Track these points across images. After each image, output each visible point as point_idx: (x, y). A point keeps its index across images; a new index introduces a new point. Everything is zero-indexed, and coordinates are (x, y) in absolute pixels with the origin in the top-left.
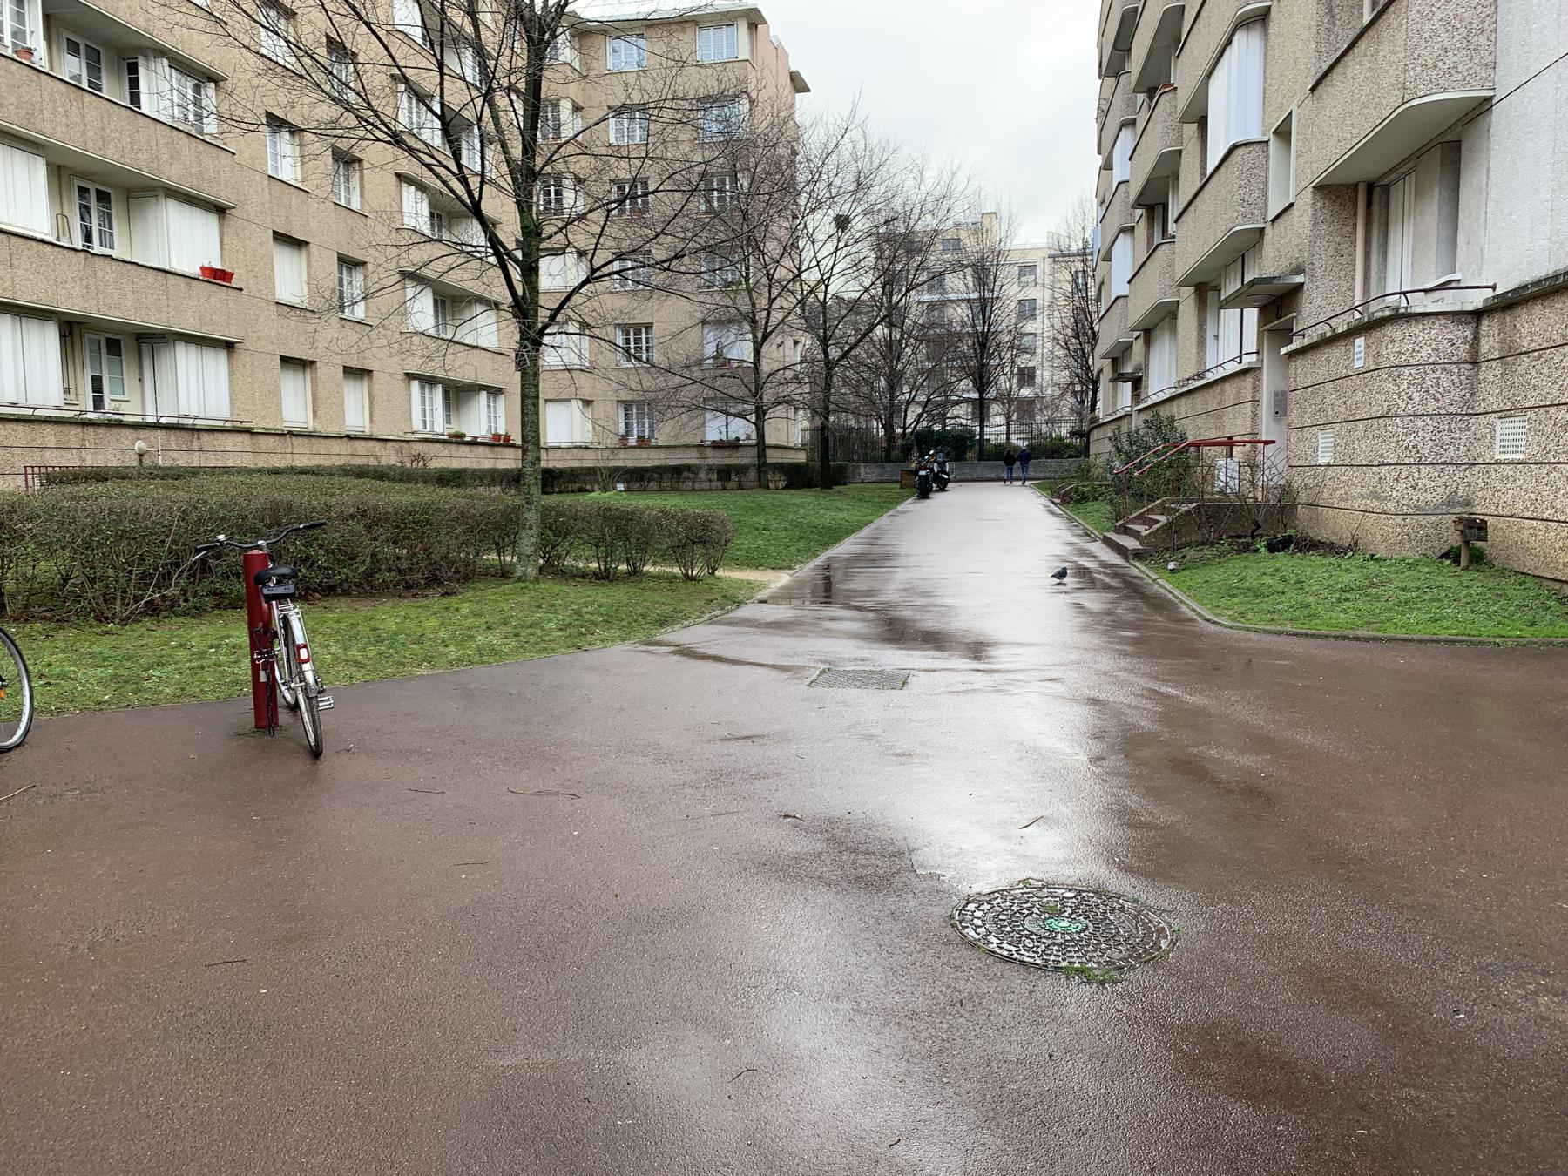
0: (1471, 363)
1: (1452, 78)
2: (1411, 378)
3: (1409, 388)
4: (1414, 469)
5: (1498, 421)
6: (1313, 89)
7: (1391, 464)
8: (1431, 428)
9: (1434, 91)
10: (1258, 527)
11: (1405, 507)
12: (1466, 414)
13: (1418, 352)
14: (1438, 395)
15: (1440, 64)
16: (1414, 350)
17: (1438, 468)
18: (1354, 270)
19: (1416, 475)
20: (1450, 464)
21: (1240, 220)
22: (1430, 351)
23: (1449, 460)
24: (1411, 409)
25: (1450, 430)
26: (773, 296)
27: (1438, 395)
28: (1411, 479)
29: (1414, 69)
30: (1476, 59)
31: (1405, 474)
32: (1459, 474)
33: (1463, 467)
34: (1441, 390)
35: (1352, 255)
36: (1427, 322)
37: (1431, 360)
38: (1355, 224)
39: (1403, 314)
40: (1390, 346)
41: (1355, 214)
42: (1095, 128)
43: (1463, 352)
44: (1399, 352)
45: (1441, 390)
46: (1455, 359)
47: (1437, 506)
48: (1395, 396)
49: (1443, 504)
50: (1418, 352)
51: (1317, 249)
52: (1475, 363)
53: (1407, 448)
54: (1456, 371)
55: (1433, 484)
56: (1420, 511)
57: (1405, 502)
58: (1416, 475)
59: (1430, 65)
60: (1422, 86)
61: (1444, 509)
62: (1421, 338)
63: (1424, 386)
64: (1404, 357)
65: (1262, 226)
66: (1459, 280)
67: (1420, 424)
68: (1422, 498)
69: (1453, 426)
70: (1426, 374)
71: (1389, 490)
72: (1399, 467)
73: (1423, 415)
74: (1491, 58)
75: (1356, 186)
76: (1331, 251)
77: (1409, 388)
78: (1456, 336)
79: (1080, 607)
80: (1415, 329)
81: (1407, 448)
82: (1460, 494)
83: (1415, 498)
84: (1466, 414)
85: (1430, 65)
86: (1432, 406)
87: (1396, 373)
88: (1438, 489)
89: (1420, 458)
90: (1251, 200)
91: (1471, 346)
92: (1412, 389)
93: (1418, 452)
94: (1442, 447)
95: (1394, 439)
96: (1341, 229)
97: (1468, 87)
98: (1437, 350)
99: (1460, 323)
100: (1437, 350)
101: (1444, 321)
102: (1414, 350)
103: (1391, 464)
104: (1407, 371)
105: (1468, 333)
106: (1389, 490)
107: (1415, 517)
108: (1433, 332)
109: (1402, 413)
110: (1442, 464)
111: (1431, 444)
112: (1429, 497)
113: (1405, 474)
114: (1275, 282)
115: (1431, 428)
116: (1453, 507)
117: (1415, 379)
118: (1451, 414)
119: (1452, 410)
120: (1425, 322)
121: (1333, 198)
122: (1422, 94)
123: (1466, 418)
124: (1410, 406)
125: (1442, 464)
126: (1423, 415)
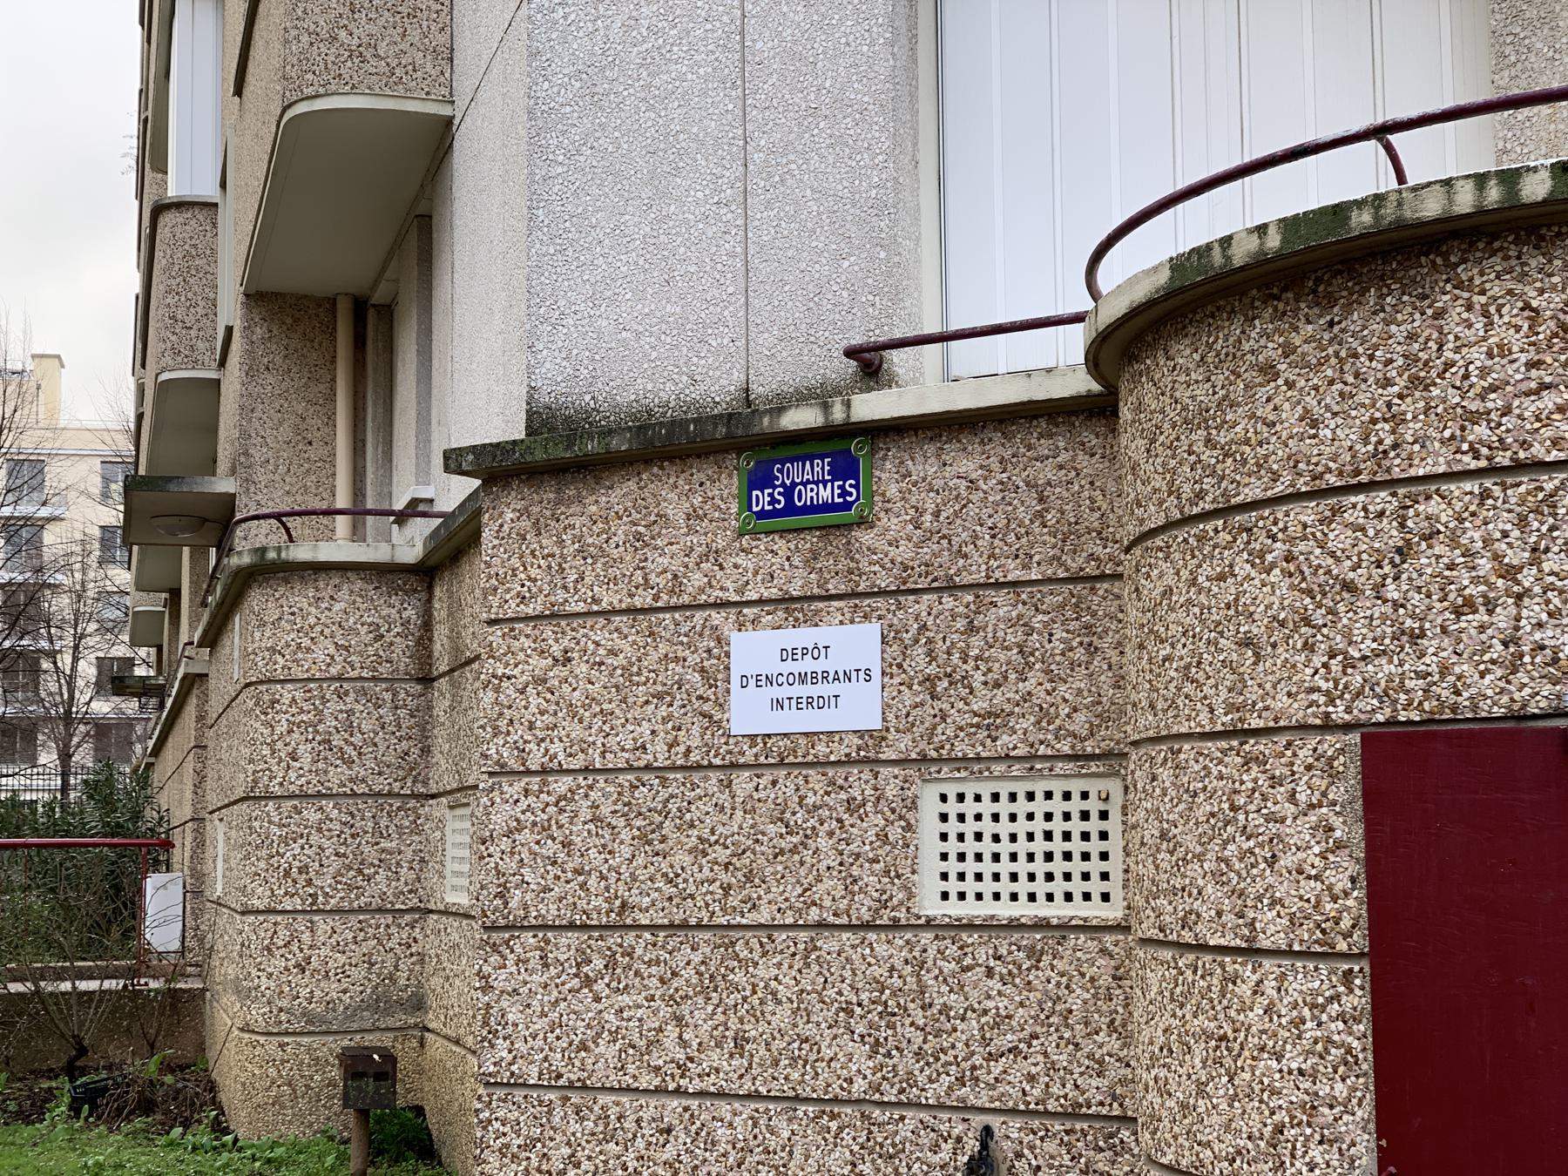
0: (419, 680)
1: (366, 66)
2: (294, 710)
3: (290, 731)
4: (301, 924)
5: (448, 814)
6: (238, 91)
7: (258, 912)
8: (337, 826)
9: (333, 88)
10: (82, 1051)
11: (283, 1017)
12: (413, 796)
13: (308, 650)
14: (349, 750)
15: (343, 34)
16: (299, 646)
17: (353, 920)
18: (334, 474)
19: (306, 937)
20: (380, 910)
21: (168, 360)
22: (332, 650)
23: (375, 904)
24: (296, 783)
25: (379, 833)
26: (291, 522)
27: (349, 750)
28: (295, 948)
29: (297, 38)
30: (415, 35)
31: (284, 934)
32: (400, 935)
33: (408, 918)
34: (357, 739)
35: (329, 442)
36: (326, 585)
37: (334, 671)
38: (334, 380)
39: (273, 563)
40: (257, 635)
41: (333, 360)
42: (136, 203)
43: (401, 653)
44: (272, 650)
45: (357, 739)
46: (384, 670)
47: (352, 1012)
48: (266, 751)
49: (365, 1006)
50: (308, 650)
51: (256, 424)
52: (427, 680)
53: (287, 873)
54: (388, 696)
55: (342, 959)
56: (315, 1025)
57: (284, 1003)
58: (306, 937)
59: (324, 34)
60: (310, 76)
61: (367, 1018)
62: (312, 620)
63: (321, 728)
64: (281, 661)
65: (213, 375)
66: (431, 501)
67: (312, 816)
68: (318, 993)
69: (383, 823)
70: (324, 701)
71: (254, 972)
72: (273, 919)
73: (319, 795)
74: (443, 39)
75: (333, 302)
76: (286, 432)
77: (290, 731)
78: (386, 618)
79: (134, 1132)
80: (300, 598)
81: (287, 873)
82: (403, 982)
83: (304, 993)
84: (413, 796)
85: (324, 34)
86: (337, 776)
87: (266, 697)
88: (353, 972)
89: (314, 896)
90: (190, 320)
91: (418, 643)
92: (296, 735)
93: (309, 882)
94: (360, 871)
95: (264, 853)
96: (306, 386)
97: (401, 90)
98: (346, 649)
99: (394, 590)
100: (346, 649)
101: (359, 584)
102: (299, 646)
103: (258, 912)
104: (286, 693)
105: (410, 613)
106: (254, 972)
107: (306, 1040)
108: (337, 607)
109: (277, 790)
110: (360, 910)
111: (335, 864)
112: (333, 989)
113: (284, 934)
114: (173, 487)
115: (337, 826)
116: (387, 1012)
117: (302, 711)
118: (379, 794)
119: (380, 784)
120: (321, 584)
121: (289, 321)
122: (309, 91)
123: (412, 803)
124: (292, 775)
125: (360, 910)
126: (319, 795)
